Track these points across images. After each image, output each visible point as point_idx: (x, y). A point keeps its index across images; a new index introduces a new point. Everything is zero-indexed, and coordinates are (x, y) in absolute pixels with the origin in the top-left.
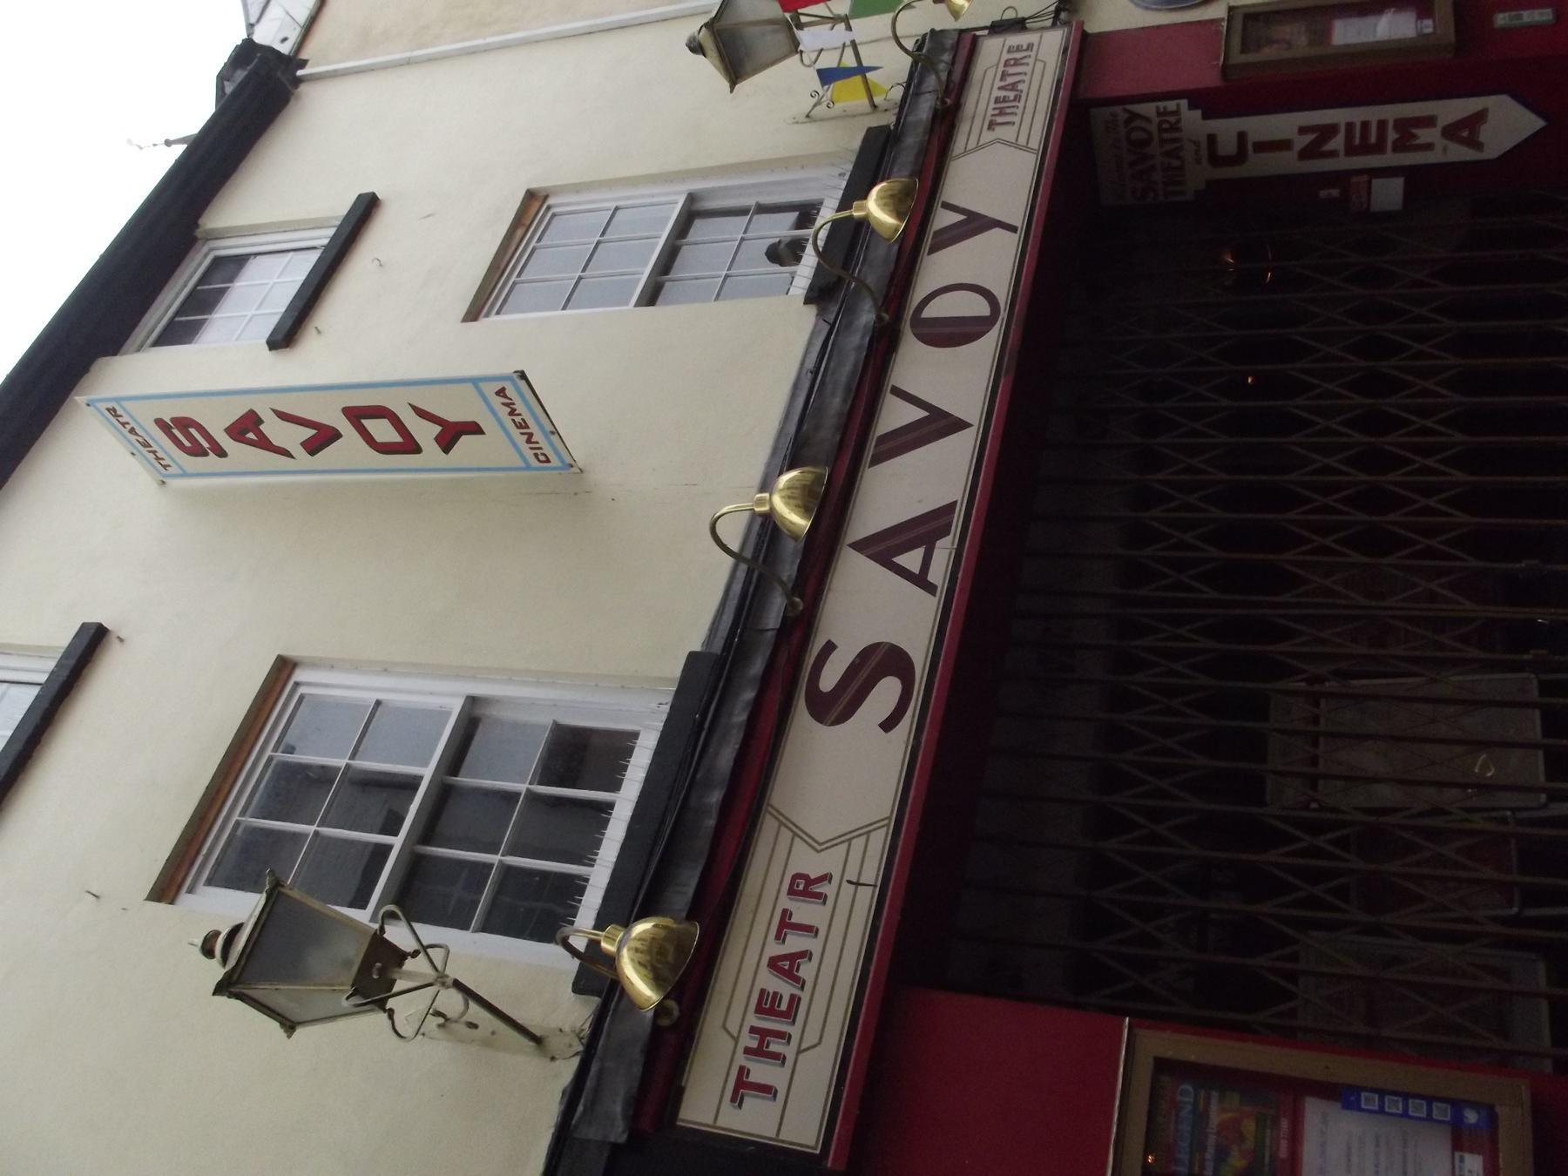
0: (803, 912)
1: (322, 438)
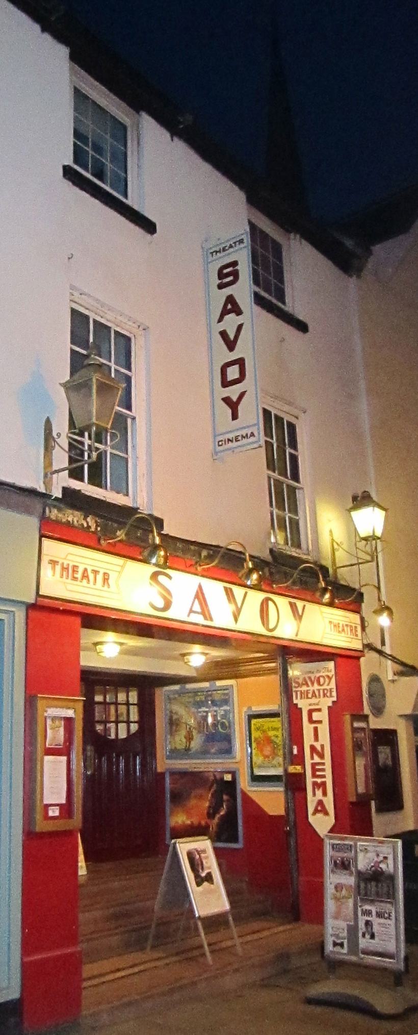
1: (231, 345)
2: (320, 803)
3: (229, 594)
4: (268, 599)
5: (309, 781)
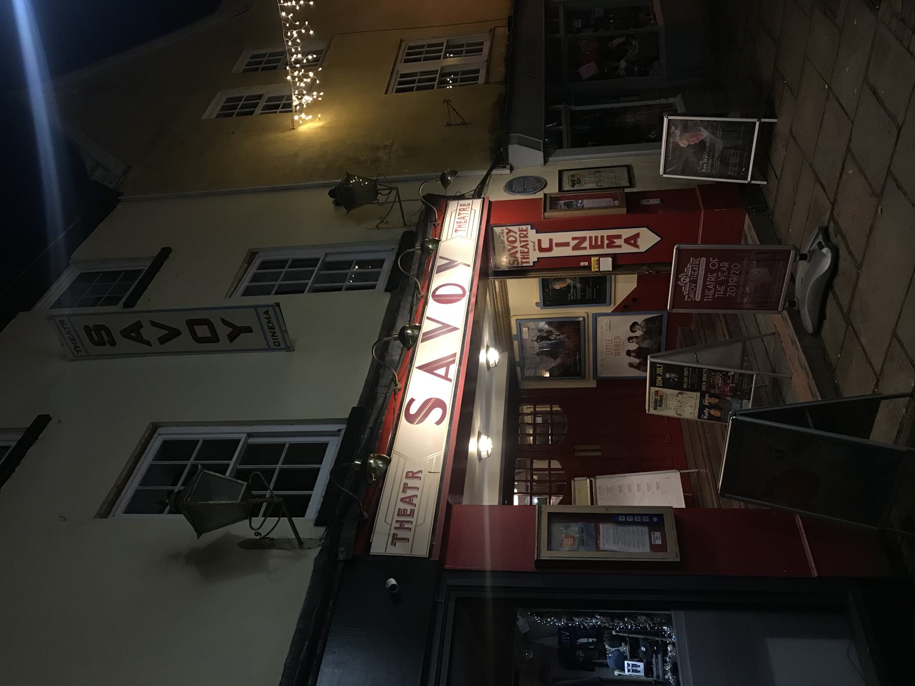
0: (412, 483)
1: (174, 333)
2: (627, 241)
3: (429, 336)
4: (434, 295)
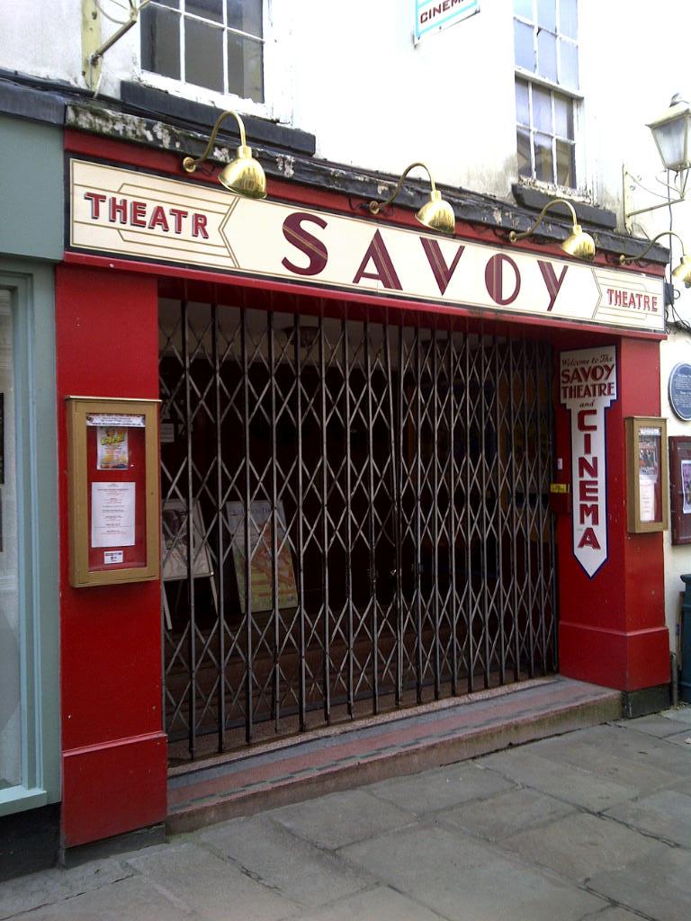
4: (500, 258)
5: (577, 503)
